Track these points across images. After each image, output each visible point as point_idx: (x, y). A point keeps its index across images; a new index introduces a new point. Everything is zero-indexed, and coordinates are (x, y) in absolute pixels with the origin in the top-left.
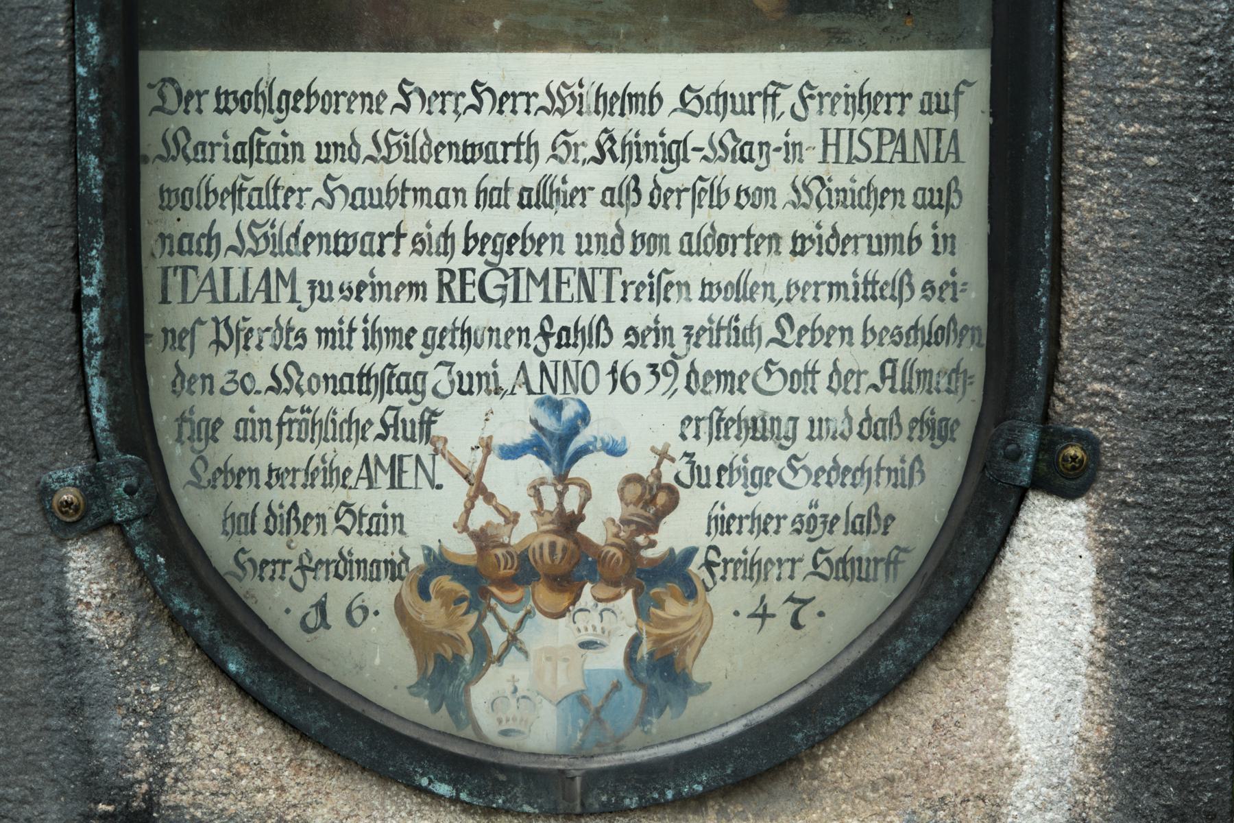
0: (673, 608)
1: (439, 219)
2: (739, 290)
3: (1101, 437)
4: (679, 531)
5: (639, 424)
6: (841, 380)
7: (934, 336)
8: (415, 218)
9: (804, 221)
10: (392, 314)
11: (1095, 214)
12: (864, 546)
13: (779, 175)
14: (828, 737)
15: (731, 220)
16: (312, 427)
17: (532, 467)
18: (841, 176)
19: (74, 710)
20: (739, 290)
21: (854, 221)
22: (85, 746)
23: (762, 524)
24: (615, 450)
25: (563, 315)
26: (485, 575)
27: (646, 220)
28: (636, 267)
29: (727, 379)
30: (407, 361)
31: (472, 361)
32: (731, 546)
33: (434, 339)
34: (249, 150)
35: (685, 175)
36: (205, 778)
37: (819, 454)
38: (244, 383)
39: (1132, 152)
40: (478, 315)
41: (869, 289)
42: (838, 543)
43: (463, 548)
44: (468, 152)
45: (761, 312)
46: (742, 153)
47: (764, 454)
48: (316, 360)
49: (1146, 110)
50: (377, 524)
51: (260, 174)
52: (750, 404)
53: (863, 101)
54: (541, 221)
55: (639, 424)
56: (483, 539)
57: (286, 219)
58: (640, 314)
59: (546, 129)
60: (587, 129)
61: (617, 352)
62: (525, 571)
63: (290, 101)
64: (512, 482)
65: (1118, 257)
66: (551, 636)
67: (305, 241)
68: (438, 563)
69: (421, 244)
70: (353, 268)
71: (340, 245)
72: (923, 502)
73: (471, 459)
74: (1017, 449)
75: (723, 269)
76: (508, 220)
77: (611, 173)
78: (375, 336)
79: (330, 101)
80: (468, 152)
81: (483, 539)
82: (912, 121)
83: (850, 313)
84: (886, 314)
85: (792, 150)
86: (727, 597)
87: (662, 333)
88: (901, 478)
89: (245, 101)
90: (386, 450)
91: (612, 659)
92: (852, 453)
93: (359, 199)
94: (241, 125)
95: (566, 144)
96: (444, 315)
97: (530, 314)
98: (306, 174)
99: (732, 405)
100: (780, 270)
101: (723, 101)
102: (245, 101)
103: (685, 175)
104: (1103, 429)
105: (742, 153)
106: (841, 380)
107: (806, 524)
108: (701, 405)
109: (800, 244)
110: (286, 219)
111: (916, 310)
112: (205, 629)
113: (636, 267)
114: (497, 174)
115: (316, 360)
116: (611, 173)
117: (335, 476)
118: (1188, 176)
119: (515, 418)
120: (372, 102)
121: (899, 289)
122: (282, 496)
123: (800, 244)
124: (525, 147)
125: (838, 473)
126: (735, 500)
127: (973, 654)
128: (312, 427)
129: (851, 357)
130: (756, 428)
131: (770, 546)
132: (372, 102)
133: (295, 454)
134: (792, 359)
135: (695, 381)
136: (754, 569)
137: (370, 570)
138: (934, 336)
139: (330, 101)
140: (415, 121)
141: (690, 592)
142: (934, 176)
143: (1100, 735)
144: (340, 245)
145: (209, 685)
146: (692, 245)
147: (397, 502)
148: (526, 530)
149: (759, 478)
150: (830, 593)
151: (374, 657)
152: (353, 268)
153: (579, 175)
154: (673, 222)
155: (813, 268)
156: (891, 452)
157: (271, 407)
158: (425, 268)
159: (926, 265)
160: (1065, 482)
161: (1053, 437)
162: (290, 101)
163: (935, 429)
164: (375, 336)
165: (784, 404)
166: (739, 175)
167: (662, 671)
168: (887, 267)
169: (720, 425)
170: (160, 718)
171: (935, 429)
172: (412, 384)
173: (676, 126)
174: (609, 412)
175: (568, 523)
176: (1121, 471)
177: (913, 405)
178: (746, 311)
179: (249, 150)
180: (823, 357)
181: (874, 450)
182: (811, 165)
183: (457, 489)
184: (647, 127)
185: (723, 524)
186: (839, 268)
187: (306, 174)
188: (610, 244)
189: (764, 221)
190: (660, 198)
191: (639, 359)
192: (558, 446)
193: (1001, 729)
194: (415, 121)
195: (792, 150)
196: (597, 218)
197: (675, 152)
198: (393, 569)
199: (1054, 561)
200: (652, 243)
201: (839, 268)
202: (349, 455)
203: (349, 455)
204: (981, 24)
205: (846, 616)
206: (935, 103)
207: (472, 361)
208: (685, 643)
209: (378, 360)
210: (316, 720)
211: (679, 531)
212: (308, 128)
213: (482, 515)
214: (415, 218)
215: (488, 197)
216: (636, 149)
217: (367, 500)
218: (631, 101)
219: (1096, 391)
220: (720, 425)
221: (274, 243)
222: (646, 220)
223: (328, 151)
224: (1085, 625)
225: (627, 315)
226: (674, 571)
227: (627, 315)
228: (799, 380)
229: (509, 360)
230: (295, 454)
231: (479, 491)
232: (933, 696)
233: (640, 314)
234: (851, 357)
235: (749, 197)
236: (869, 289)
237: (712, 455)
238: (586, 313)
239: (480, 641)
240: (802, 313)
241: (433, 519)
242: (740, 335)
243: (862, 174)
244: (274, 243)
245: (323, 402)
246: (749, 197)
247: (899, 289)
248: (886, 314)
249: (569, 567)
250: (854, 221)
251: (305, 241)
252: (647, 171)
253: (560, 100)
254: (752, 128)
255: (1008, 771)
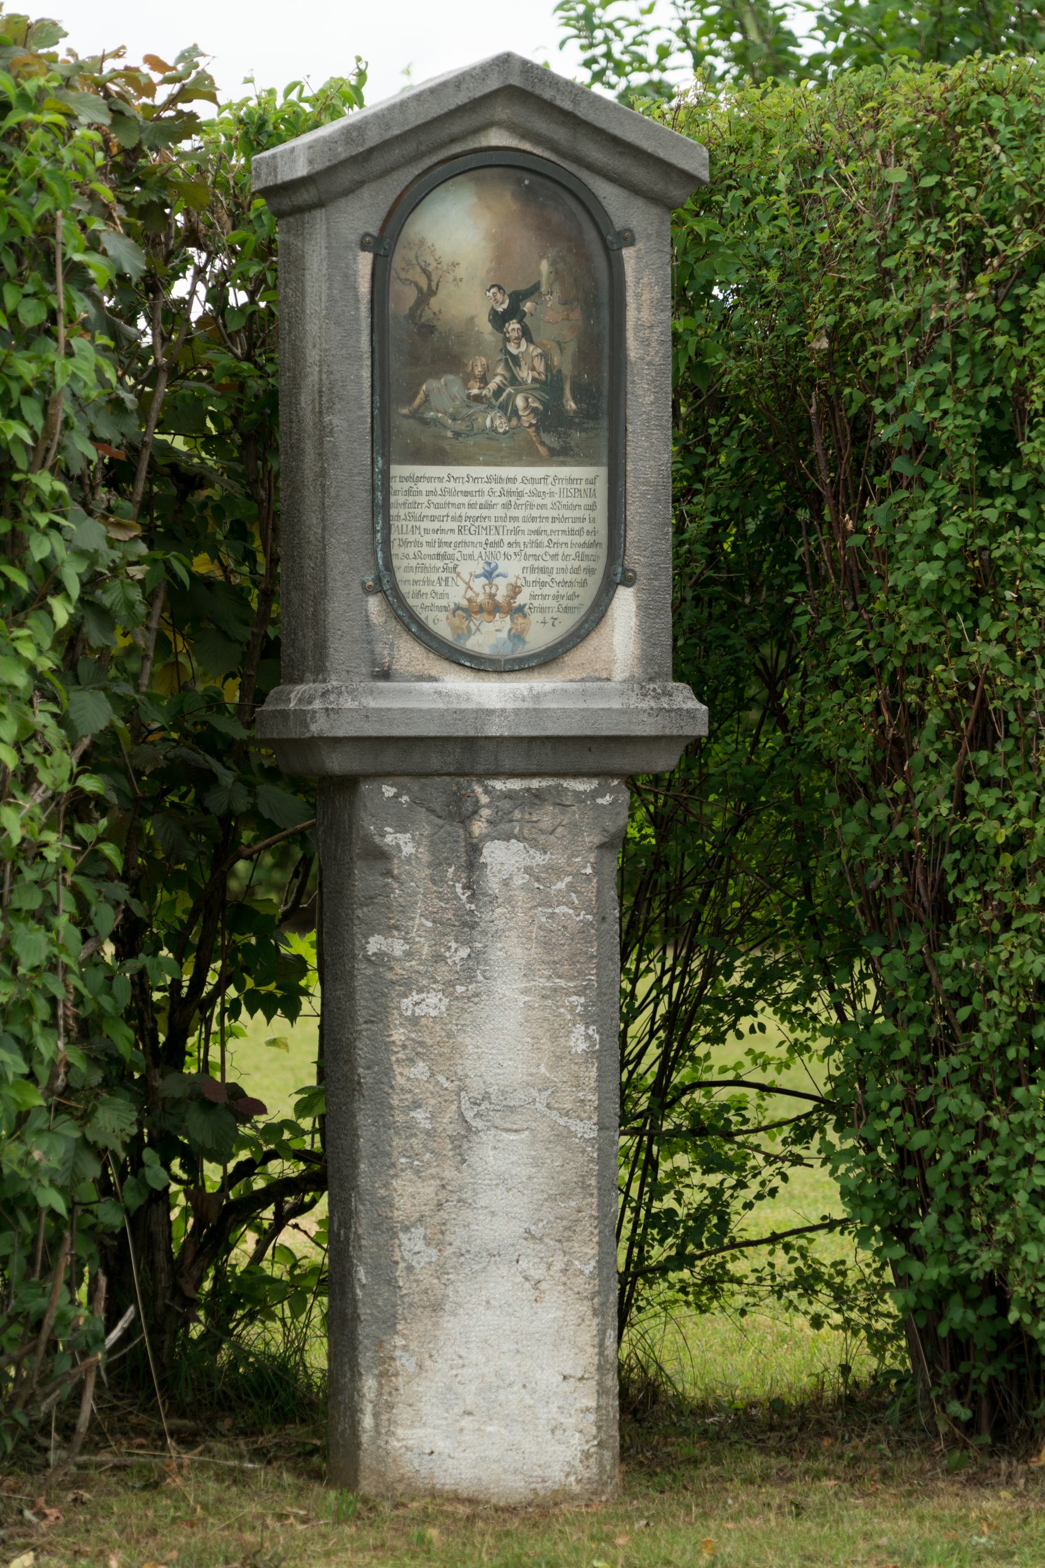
0: (521, 620)
1: (458, 512)
2: (538, 532)
3: (517, 815)
4: (521, 599)
5: (512, 569)
6: (565, 557)
7: (591, 545)
8: (452, 511)
9: (555, 513)
10: (446, 538)
11: (635, 510)
12: (570, 603)
13: (548, 501)
14: (567, 651)
15: (535, 513)
16: (424, 569)
17: (483, 581)
18: (564, 501)
19: (369, 642)
20: (538, 532)
21: (568, 514)
22: (372, 652)
23: (544, 597)
24: (505, 576)
25: (491, 539)
26: (471, 610)
27: (513, 512)
28: (510, 526)
29: (536, 557)
30: (450, 551)
31: (467, 551)
32: (536, 603)
33: (458, 544)
34: (409, 492)
35: (523, 500)
36: (404, 661)
37: (559, 578)
38: (407, 557)
39: (644, 494)
40: (469, 538)
41: (572, 532)
42: (565, 602)
43: (464, 603)
44: (466, 494)
45: (544, 538)
46: (538, 494)
47: (544, 577)
48: (426, 550)
49: (647, 483)
50: (442, 596)
51: (411, 499)
52: (541, 564)
53: (571, 481)
54: (485, 512)
55: (512, 569)
56: (469, 600)
57: (418, 512)
58: (511, 538)
59: (486, 487)
60: (497, 487)
61: (505, 549)
62: (481, 610)
63: (419, 479)
64: (478, 584)
65: (641, 522)
66: (488, 628)
67: (422, 518)
68: (458, 608)
69: (453, 519)
70: (436, 525)
71: (433, 518)
72: (587, 596)
73: (466, 578)
74: (615, 576)
75: (534, 526)
76: (476, 512)
77: (504, 500)
78: (441, 544)
79: (429, 479)
80: (466, 494)
81: (469, 600)
82: (583, 486)
83: (568, 539)
84: (577, 539)
85: (552, 494)
86: (535, 617)
87: (517, 543)
88: (583, 584)
89: (406, 479)
90: (444, 575)
91: (504, 635)
92: (568, 577)
93: (437, 506)
94: (406, 486)
95: (492, 492)
96: (458, 538)
97: (482, 538)
98: (423, 499)
99: (536, 564)
100: (548, 526)
101: (533, 480)
102: (406, 479)
103: (523, 500)
104: (638, 569)
105: (538, 494)
106: (565, 557)
107: (556, 597)
108: (528, 564)
109: (554, 519)
110: (418, 512)
111: (585, 538)
112: (406, 620)
113: (510, 526)
114: (473, 500)
115: (426, 550)
116: (504, 500)
117: (429, 582)
118: (658, 501)
119: (479, 567)
120: (440, 479)
121: (580, 532)
122: (417, 588)
123: (554, 519)
124: (480, 492)
125: (565, 583)
126: (537, 590)
127: (604, 629)
128: (424, 569)
129: (569, 551)
130: (542, 570)
131: (546, 603)
132: (440, 479)
133: (420, 576)
134: (552, 551)
135: (526, 557)
136: (542, 610)
137: (441, 609)
138: (591, 545)
139: (429, 479)
140: (452, 485)
141: (525, 616)
142: (589, 501)
143: (638, 652)
144: (433, 518)
145: (405, 636)
146: (525, 520)
147: (447, 590)
148: (481, 598)
149: (543, 584)
150: (562, 616)
151: (443, 629)
152: (436, 525)
153: (495, 500)
154: (520, 513)
155: (558, 526)
156: (579, 577)
157: (413, 563)
158: (454, 525)
159: (587, 526)
160: (628, 581)
161: (625, 571)
162: (419, 479)
163: (591, 571)
164: (441, 544)
165: (550, 564)
166: (537, 501)
167: (517, 637)
168: (577, 526)
169: (533, 570)
170: (392, 645)
171: (591, 571)
172: (451, 557)
173: (521, 487)
174: (503, 565)
175: (492, 596)
176: (642, 580)
177: (584, 564)
178: (540, 538)
179: (409, 492)
180: (560, 551)
181: (574, 577)
182: (556, 498)
183: (463, 586)
184: (513, 487)
185: (534, 597)
186: (564, 526)
187: (423, 499)
188: (503, 519)
189: (544, 513)
190: (517, 506)
191: (511, 551)
192: (489, 575)
193: (612, 650)
194: (452, 485)
195: (552, 494)
196: (499, 512)
197: (520, 494)
198: (446, 609)
199: (625, 604)
200: (515, 519)
201: (564, 526)
202: (434, 577)
203: (434, 577)
204: (605, 460)
205: (567, 623)
206: (592, 482)
207: (467, 551)
208: (523, 631)
209: (442, 550)
210: (434, 644)
211: (521, 599)
212: (424, 486)
213: (470, 594)
214: (452, 511)
215: (471, 506)
216: (510, 493)
217: (439, 589)
218: (509, 480)
219: (635, 558)
220: (533, 570)
221: (413, 517)
222: (513, 512)
223: (429, 493)
224: (633, 622)
225: (508, 538)
226: (520, 609)
227: (508, 538)
228: (554, 557)
229: (477, 551)
230: (420, 576)
231: (470, 587)
232: (594, 641)
233: (511, 538)
234: (569, 551)
235: (543, 506)
236: (572, 532)
237: (531, 577)
238: (497, 538)
239: (469, 628)
240: (554, 538)
241: (457, 595)
242: (539, 545)
243: (570, 500)
244: (413, 517)
245: (428, 562)
246: (543, 506)
247: (580, 532)
248: (577, 539)
249: (493, 609)
250: (568, 514)
251: (422, 518)
252: (513, 499)
253: (489, 480)
254: (541, 488)
255: (613, 662)
